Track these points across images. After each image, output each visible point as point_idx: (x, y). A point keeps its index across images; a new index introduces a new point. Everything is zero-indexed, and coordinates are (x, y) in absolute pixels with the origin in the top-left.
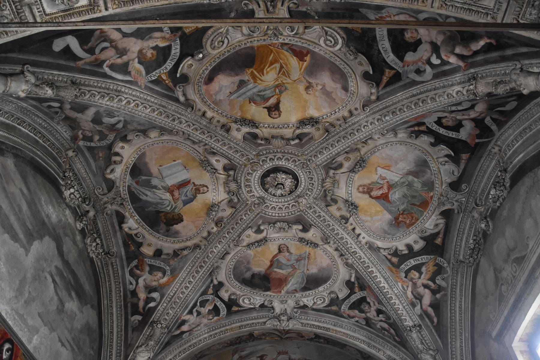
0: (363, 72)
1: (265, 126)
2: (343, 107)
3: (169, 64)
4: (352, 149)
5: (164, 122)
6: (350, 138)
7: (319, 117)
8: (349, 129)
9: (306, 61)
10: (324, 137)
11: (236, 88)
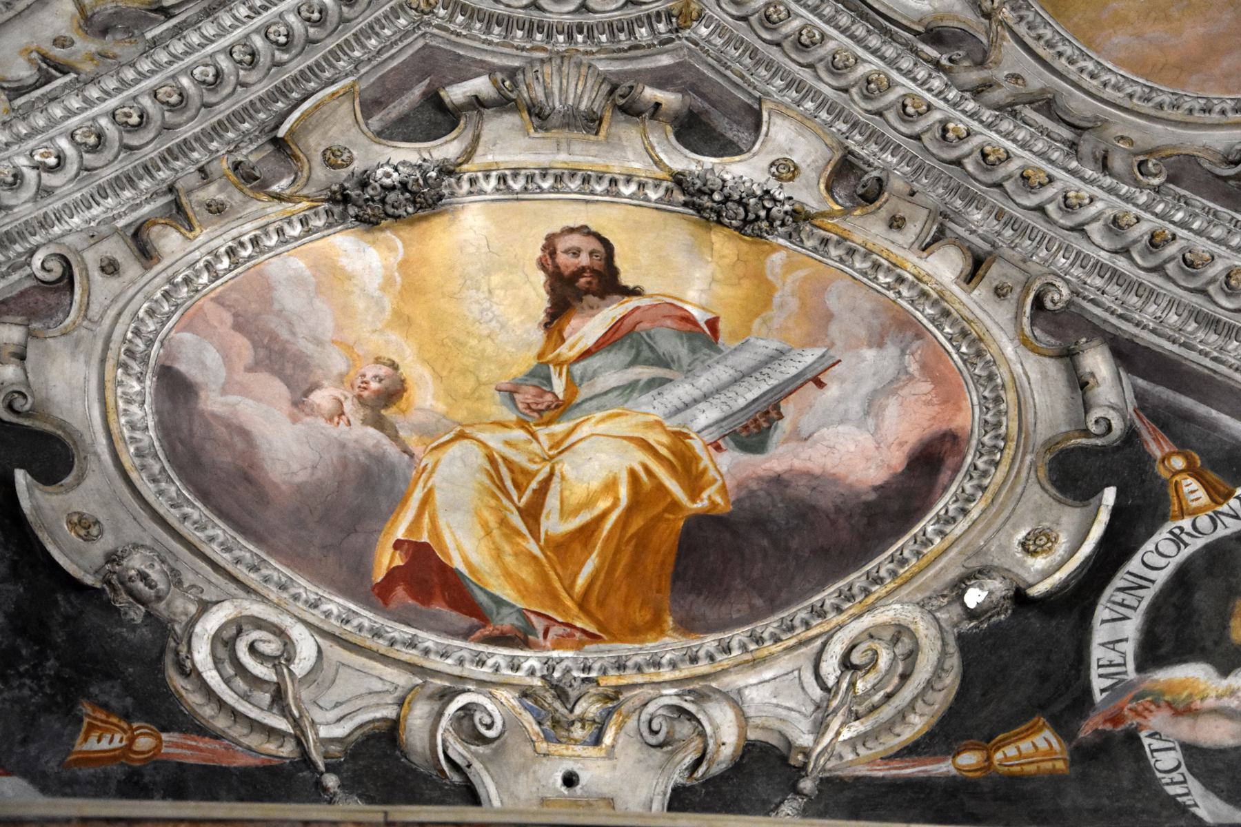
0: (69, 480)
1: (633, 188)
2: (187, 281)
3: (1161, 562)
4: (127, 30)
5: (1217, 232)
6: (147, 102)
7: (329, 226)
8: (151, 153)
9: (398, 545)
10: (296, 114)
11: (789, 408)
